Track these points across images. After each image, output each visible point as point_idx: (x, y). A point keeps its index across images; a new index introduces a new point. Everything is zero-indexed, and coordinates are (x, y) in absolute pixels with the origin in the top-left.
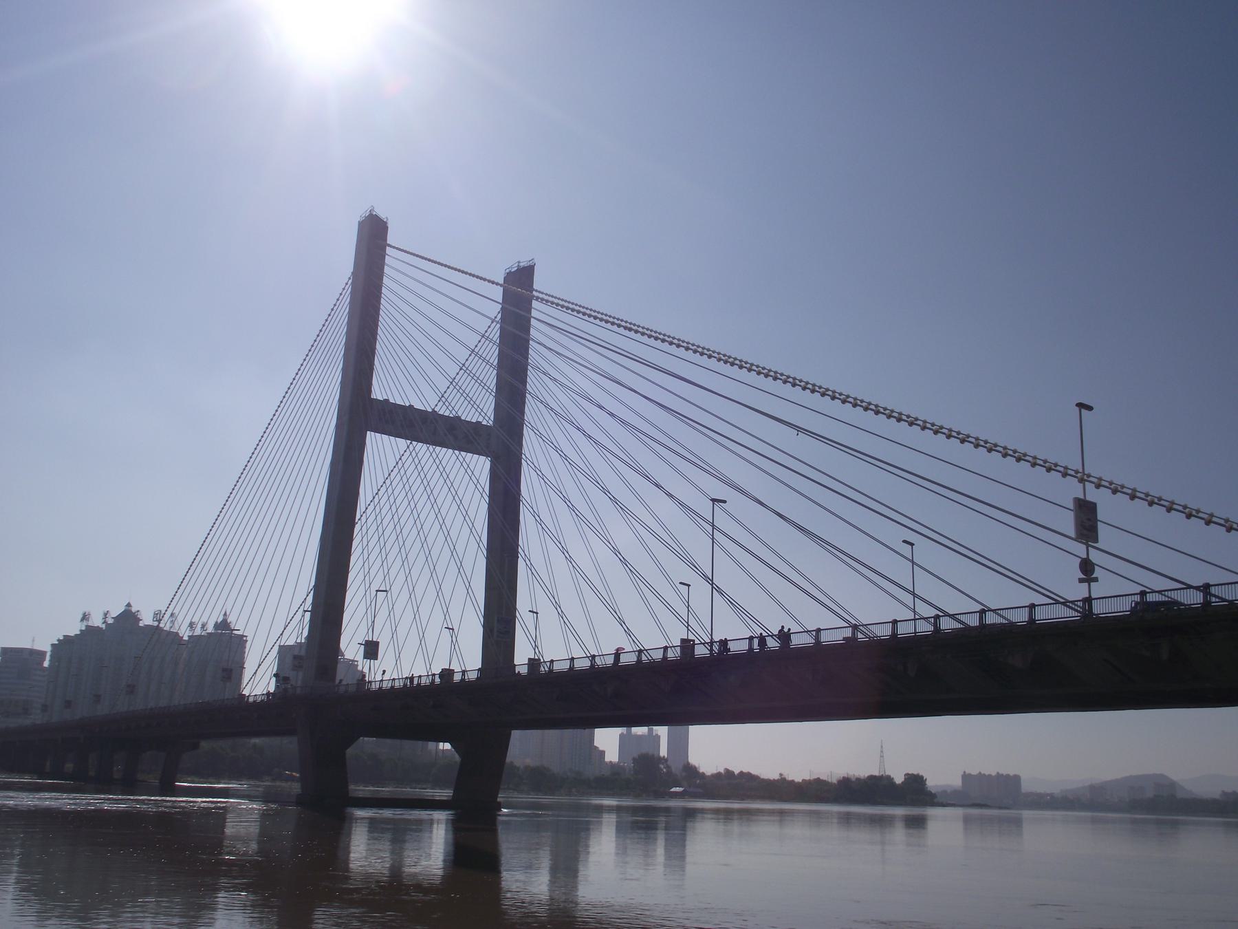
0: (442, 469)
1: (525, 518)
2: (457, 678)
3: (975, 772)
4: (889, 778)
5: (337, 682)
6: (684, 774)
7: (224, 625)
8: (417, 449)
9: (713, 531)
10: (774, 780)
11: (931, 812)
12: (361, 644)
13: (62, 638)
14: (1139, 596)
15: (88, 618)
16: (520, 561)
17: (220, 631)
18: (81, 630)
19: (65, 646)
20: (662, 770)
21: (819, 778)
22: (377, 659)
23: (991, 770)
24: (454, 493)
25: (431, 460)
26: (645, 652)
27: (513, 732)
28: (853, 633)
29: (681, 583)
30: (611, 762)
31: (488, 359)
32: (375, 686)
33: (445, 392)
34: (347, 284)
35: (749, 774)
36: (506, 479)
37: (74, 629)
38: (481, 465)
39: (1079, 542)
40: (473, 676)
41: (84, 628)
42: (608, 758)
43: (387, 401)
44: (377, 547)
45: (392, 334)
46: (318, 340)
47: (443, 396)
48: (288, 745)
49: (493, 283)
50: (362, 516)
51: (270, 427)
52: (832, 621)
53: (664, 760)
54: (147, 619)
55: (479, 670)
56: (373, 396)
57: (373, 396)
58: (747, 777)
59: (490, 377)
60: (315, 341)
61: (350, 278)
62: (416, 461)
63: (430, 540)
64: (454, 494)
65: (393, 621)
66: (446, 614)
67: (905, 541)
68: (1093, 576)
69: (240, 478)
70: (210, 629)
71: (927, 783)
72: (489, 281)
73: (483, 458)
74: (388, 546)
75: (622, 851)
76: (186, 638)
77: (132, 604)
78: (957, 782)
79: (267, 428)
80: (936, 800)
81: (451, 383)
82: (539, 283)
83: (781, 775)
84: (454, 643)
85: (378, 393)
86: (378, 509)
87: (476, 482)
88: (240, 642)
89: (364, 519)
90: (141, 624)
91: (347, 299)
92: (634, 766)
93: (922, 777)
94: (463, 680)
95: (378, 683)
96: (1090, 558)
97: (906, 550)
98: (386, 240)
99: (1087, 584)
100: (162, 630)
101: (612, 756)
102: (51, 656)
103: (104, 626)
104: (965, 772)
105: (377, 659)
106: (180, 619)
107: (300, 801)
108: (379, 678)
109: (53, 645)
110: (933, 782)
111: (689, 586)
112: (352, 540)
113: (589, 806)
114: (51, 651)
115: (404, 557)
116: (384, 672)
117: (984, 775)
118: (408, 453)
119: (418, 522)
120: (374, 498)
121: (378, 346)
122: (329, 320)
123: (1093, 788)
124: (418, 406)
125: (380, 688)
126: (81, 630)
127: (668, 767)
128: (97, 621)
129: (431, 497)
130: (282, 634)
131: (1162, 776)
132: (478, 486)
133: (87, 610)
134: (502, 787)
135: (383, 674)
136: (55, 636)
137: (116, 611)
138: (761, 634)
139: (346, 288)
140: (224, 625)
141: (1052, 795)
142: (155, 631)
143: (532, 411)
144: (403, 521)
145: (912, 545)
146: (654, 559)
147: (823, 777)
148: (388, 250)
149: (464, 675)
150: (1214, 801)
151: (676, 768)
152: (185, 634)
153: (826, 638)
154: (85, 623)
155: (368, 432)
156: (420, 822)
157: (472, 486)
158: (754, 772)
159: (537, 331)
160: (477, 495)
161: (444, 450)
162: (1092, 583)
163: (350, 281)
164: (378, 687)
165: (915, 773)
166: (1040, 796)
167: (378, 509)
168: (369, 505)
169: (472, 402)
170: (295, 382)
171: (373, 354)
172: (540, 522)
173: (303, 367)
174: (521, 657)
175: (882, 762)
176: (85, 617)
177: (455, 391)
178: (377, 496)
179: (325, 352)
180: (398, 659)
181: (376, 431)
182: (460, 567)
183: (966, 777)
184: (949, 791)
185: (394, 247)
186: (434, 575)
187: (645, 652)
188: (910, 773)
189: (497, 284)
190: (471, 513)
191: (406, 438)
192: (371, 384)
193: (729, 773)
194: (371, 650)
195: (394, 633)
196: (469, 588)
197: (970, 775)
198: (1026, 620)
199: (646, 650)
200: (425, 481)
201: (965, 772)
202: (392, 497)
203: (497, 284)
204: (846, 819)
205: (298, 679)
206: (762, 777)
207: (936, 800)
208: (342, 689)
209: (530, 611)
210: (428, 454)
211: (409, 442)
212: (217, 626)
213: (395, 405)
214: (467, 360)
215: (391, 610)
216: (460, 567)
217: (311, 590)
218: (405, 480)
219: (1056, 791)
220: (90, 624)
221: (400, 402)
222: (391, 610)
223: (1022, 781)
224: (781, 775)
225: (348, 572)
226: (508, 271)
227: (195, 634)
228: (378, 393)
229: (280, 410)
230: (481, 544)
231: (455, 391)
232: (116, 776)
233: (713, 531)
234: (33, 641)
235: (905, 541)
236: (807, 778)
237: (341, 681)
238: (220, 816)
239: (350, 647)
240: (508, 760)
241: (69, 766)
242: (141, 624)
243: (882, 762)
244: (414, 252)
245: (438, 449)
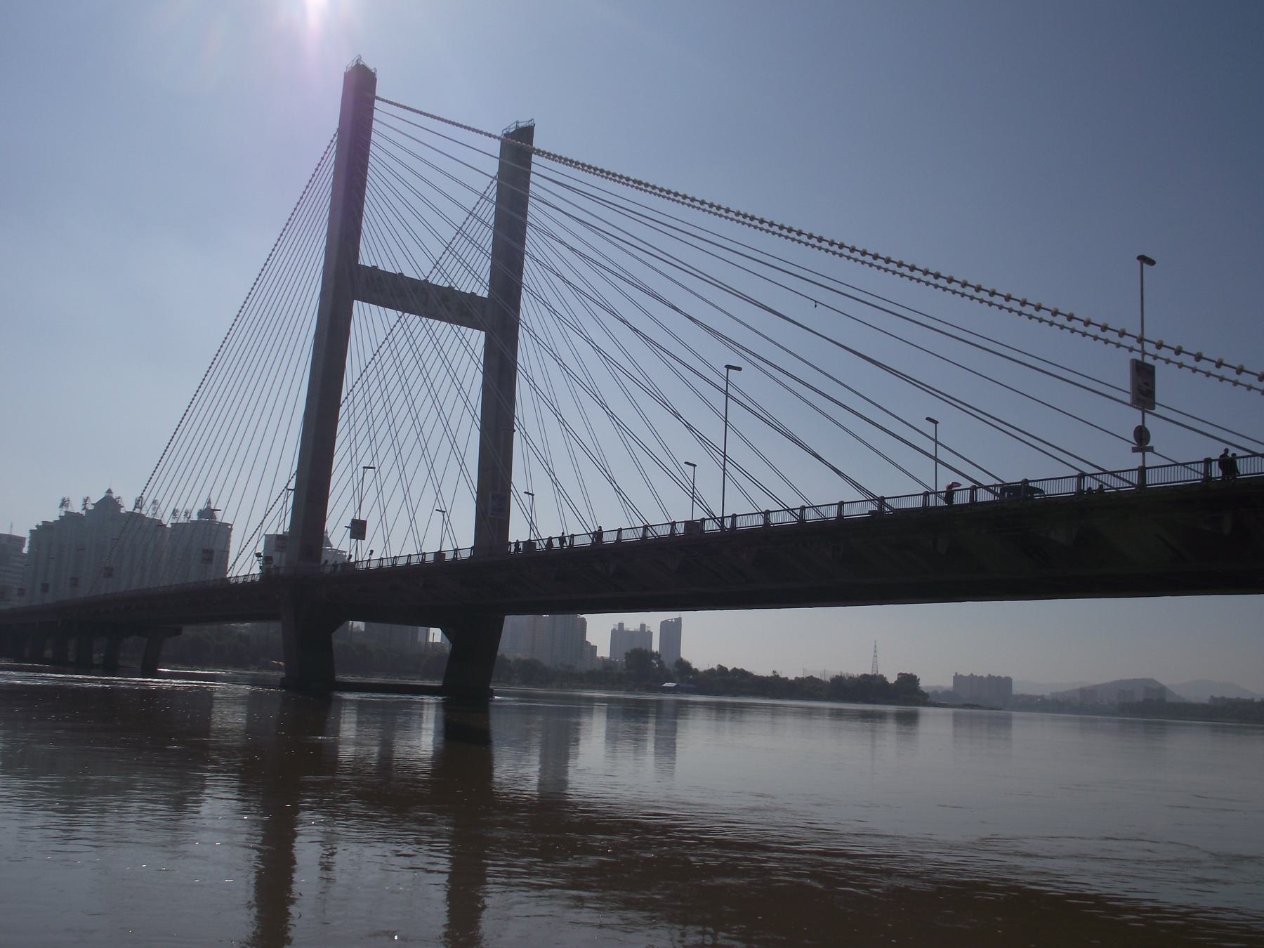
0: (435, 341)
1: (522, 388)
2: (449, 556)
3: (966, 674)
4: (882, 678)
5: (322, 563)
6: (676, 669)
7: (208, 513)
8: (409, 321)
9: (727, 387)
10: (767, 677)
11: (922, 710)
12: (348, 527)
13: (40, 524)
14: (1203, 464)
15: (67, 504)
16: (516, 435)
17: (204, 519)
18: (60, 517)
19: (44, 532)
20: (655, 665)
21: (812, 676)
22: (364, 539)
23: (982, 671)
24: (448, 366)
25: (424, 332)
26: (649, 528)
27: (506, 617)
28: (880, 507)
29: (686, 463)
30: (602, 657)
31: (486, 221)
32: (362, 566)
33: (441, 258)
34: (332, 141)
35: (743, 671)
36: (505, 349)
37: (53, 515)
38: (477, 338)
39: (1135, 407)
40: (465, 554)
41: (63, 514)
42: (599, 654)
43: (375, 268)
44: (365, 426)
45: (377, 189)
46: (301, 203)
47: (437, 263)
48: (270, 632)
49: (490, 135)
50: (348, 394)
51: (251, 296)
52: (851, 494)
53: (657, 656)
54: (128, 506)
55: (472, 548)
56: (361, 262)
57: (361, 262)
58: (741, 674)
59: (486, 238)
60: (298, 203)
61: (335, 135)
62: (408, 334)
63: (422, 417)
64: (446, 361)
65: (381, 503)
66: (438, 492)
67: (928, 419)
68: (1147, 446)
69: (219, 351)
70: (195, 517)
71: (920, 682)
72: (486, 134)
73: (477, 332)
74: (377, 424)
75: (612, 738)
76: (169, 526)
78: (948, 683)
79: (248, 298)
80: (928, 700)
81: (447, 248)
82: (537, 143)
83: (774, 672)
84: (446, 523)
85: (366, 259)
86: (366, 387)
87: (471, 352)
88: (225, 531)
89: (350, 397)
90: (122, 511)
91: (332, 159)
92: (626, 662)
93: (915, 677)
94: (455, 559)
95: (365, 563)
96: (1146, 426)
97: (929, 428)
98: (374, 92)
99: (1141, 454)
100: (142, 517)
101: (604, 651)
102: (30, 542)
104: (956, 674)
105: (363, 538)
106: (163, 507)
107: (283, 684)
108: (367, 558)
109: (32, 531)
110: (925, 683)
111: (695, 466)
112: (336, 421)
113: (580, 698)
114: (30, 537)
115: (394, 435)
116: (372, 551)
117: (976, 676)
118: (399, 325)
119: (409, 398)
120: (362, 375)
121: (365, 208)
122: (316, 174)
123: (1084, 692)
124: (409, 273)
125: (368, 568)
126: (60, 517)
127: (660, 663)
128: (77, 507)
129: (424, 371)
130: (261, 523)
131: (1152, 681)
132: (474, 356)
133: (66, 496)
134: (493, 680)
135: (371, 554)
136: (34, 522)
137: (97, 497)
139: (331, 146)
140: (208, 513)
141: (1042, 697)
142: (134, 517)
143: (531, 274)
144: (390, 388)
145: (936, 422)
146: (640, 469)
147: (816, 676)
148: (377, 103)
149: (456, 554)
150: (1204, 706)
151: (669, 662)
152: (168, 521)
153: (849, 511)
154: (64, 509)
155: (355, 301)
156: (409, 704)
157: (467, 356)
158: (747, 669)
159: (537, 186)
160: (473, 366)
161: (437, 322)
162: (1146, 453)
163: (336, 138)
164: (365, 567)
165: (909, 673)
166: (1031, 698)
167: (366, 387)
168: (357, 383)
169: (469, 268)
170: (277, 248)
171: (361, 216)
172: (534, 386)
173: (288, 227)
174: (518, 532)
175: (875, 663)
176: (64, 503)
177: (451, 256)
178: (365, 373)
179: (312, 211)
180: (387, 542)
182: (453, 444)
183: (958, 678)
184: (940, 692)
185: (383, 100)
186: (426, 452)
187: (649, 528)
188: (904, 672)
189: (495, 137)
190: (466, 386)
191: (397, 309)
192: (358, 248)
193: (722, 669)
194: (358, 529)
195: (383, 515)
196: (462, 464)
197: (961, 676)
198: (1074, 491)
199: (651, 526)
200: (417, 355)
201: (956, 674)
202: (381, 373)
203: (495, 137)
204: (838, 714)
205: (279, 559)
206: (755, 674)
207: (928, 700)
208: (328, 570)
209: (525, 492)
210: (421, 325)
211: (400, 313)
212: (201, 514)
213: (384, 272)
214: (464, 223)
215: (380, 492)
216: (453, 444)
217: (294, 475)
218: (395, 354)
219: (1047, 693)
220: (70, 509)
221: (389, 269)
222: (380, 492)
223: (1013, 684)
224: (774, 672)
225: (332, 455)
226: (505, 132)
227: (179, 522)
228: (366, 259)
229: (261, 278)
230: (475, 418)
231: (451, 256)
232: (96, 662)
233: (727, 387)
234: (12, 526)
235: (928, 419)
236: (801, 676)
237: (326, 561)
238: (204, 700)
239: (337, 536)
240: (499, 653)
241: (48, 653)
242: (122, 511)
243: (875, 663)
244: (404, 104)
245: (431, 321)
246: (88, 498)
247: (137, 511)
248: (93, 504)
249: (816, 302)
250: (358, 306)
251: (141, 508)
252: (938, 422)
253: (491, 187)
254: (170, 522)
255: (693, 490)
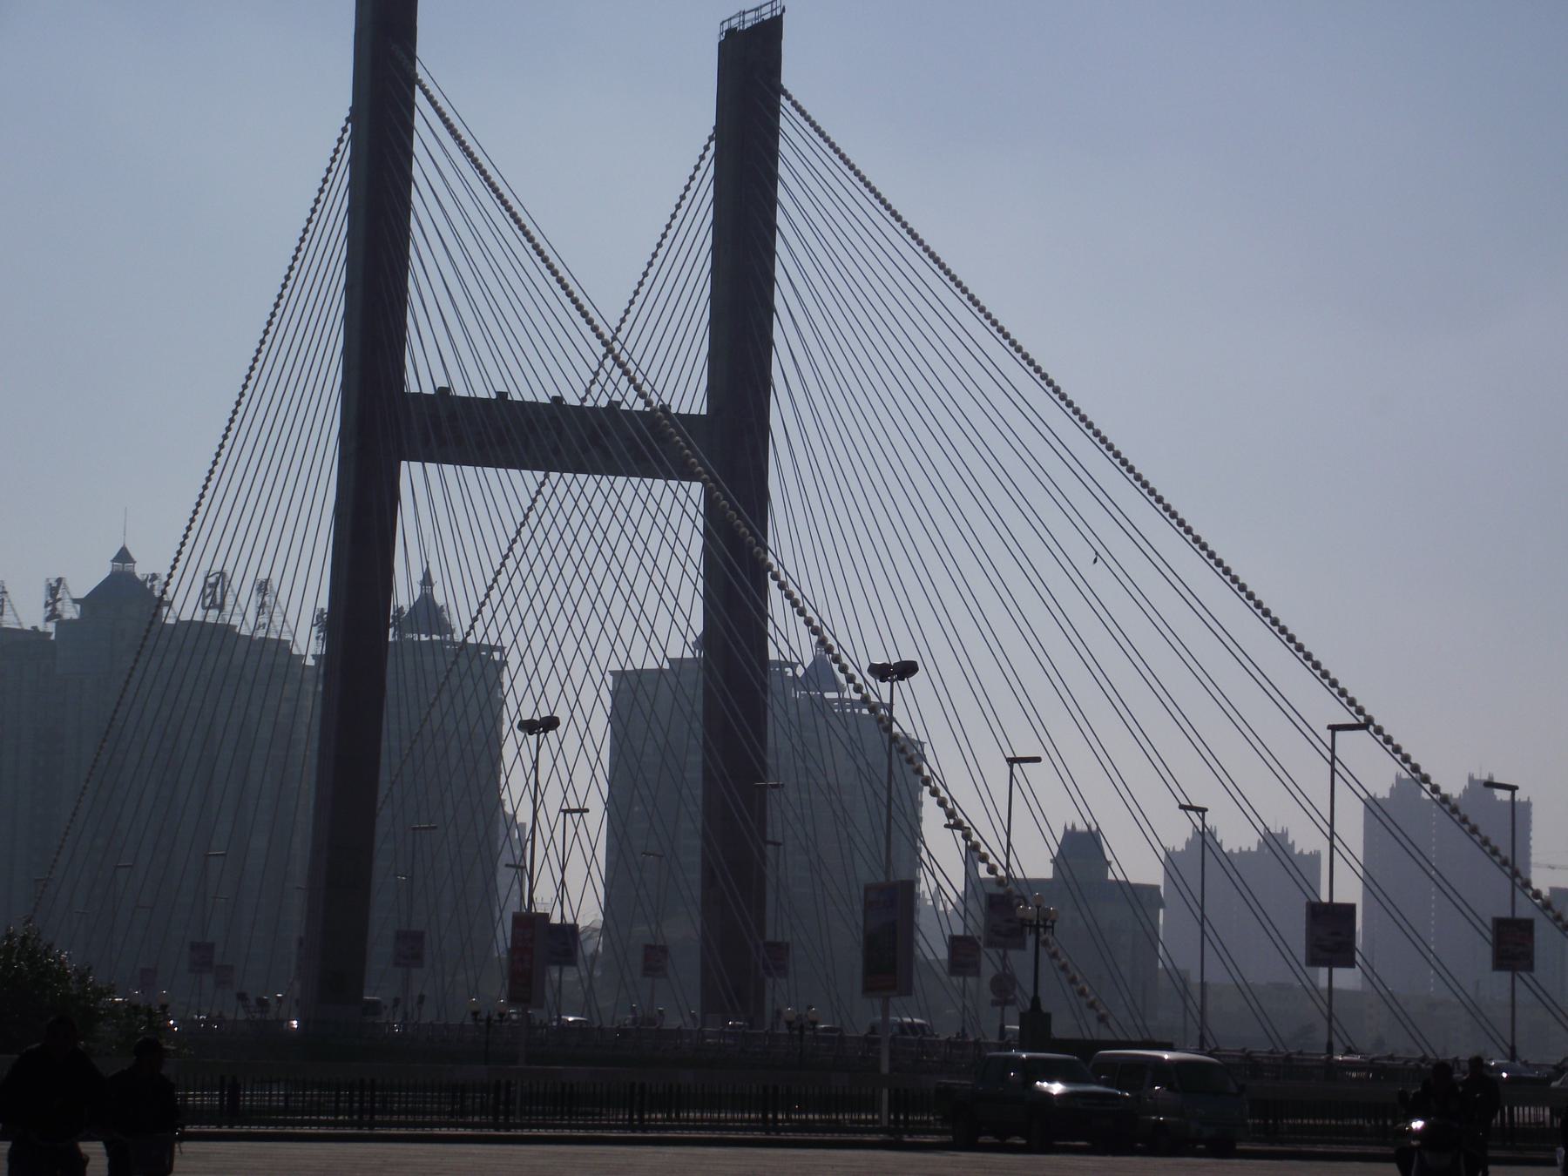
51: (224, 452)
54: (185, 606)
61: (344, 130)
77: (134, 554)
100: (228, 629)
103: (51, 627)
137: (86, 577)
138: (980, 1039)
155: (404, 464)
181: (425, 458)
226: (726, 27)
245: (582, 477)
246: (59, 581)
247: (212, 616)
248: (75, 601)
249: (1097, 553)
250: (411, 474)
251: (221, 607)
252: (1206, 810)
253: (704, 165)
254: (311, 652)
255: (1008, 856)
